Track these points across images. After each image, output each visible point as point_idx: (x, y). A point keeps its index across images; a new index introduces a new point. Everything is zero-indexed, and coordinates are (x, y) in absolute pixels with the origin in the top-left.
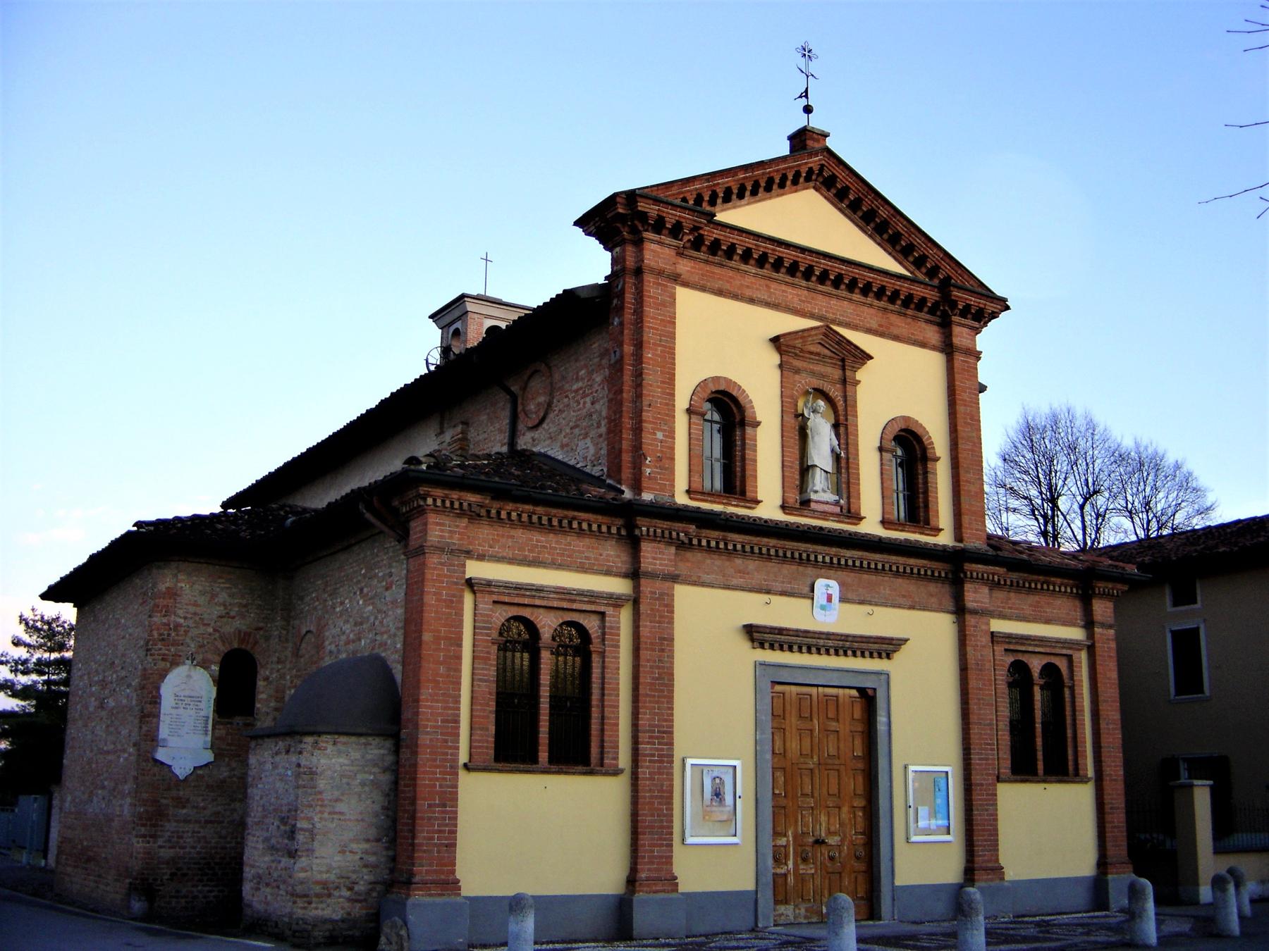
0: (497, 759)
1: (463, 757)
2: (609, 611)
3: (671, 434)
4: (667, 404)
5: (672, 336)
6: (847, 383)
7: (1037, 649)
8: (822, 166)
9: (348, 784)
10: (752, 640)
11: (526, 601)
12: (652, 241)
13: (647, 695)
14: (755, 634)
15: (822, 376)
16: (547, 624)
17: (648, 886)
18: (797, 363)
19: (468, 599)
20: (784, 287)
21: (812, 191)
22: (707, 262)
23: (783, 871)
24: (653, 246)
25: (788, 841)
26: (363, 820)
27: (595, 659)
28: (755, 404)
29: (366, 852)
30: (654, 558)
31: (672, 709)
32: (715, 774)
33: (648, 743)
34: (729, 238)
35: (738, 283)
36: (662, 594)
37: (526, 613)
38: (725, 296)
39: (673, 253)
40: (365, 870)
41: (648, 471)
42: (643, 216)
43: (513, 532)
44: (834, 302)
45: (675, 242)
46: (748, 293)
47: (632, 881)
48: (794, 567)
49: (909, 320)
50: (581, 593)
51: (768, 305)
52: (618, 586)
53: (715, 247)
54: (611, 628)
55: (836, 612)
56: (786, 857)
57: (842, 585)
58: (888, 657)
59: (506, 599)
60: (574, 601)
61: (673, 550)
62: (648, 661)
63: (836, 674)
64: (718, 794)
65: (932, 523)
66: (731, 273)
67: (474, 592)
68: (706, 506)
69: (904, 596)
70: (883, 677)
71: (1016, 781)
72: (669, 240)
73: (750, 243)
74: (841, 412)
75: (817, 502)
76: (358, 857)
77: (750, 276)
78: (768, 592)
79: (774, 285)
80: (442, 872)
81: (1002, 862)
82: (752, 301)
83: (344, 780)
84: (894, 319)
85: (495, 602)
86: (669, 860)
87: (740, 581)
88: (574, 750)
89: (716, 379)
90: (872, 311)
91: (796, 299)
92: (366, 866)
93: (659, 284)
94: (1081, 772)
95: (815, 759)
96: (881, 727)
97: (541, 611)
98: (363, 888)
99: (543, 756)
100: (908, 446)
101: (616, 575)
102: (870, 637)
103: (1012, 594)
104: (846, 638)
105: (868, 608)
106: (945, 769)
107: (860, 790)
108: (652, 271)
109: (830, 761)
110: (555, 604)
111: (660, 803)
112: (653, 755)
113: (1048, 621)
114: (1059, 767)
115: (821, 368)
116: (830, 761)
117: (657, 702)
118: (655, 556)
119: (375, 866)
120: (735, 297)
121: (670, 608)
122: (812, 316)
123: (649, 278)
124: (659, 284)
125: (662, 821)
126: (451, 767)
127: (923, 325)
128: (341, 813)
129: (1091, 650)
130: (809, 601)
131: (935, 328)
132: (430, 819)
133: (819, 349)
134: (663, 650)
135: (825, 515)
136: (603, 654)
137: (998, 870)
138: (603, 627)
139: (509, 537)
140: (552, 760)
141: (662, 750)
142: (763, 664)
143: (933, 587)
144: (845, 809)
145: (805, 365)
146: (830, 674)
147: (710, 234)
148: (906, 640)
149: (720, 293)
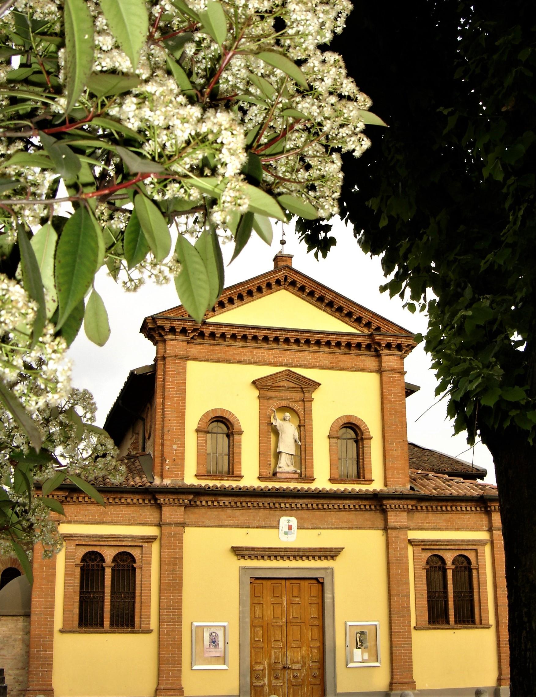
0: (80, 625)
1: (413, 624)
2: (145, 545)
3: (182, 445)
4: (180, 429)
5: (184, 391)
6: (306, 401)
7: (448, 547)
8: (286, 276)
9: (7, 640)
10: (237, 555)
11: (95, 543)
12: (387, 355)
13: (166, 589)
14: (240, 552)
15: (287, 399)
16: (109, 554)
17: (165, 692)
18: (270, 394)
19: (410, 548)
20: (262, 351)
21: (283, 291)
22: (210, 344)
23: (260, 684)
24: (172, 342)
25: (265, 667)
26: (15, 659)
27: (474, 572)
28: (240, 421)
29: (17, 675)
30: (171, 515)
31: (181, 596)
32: (212, 630)
33: (166, 615)
34: (219, 331)
35: (231, 353)
36: (175, 534)
37: (463, 553)
38: (221, 362)
39: (185, 344)
40: (16, 684)
41: (167, 467)
42: (162, 328)
43: (88, 507)
44: (298, 354)
45: (399, 353)
46: (238, 358)
47: (391, 684)
48: (268, 511)
49: (354, 356)
50: (126, 537)
51: (250, 363)
52: (151, 531)
53: (213, 335)
54: (146, 554)
55: (295, 536)
56: (264, 676)
57: (299, 519)
58: (332, 558)
59: (84, 543)
60: (123, 541)
61: (182, 509)
62: (166, 571)
63: (295, 571)
64: (214, 642)
65: (367, 477)
66: (226, 348)
67: (412, 545)
68: (211, 483)
69: (346, 522)
70: (329, 571)
71: (114, 632)
72: (181, 337)
73: (234, 331)
74: (302, 418)
75: (281, 473)
76: (13, 677)
77: (239, 349)
78: (248, 527)
79: (255, 351)
80: (44, 685)
81: (415, 678)
82: (239, 362)
83: (5, 639)
84: (341, 357)
85: (77, 545)
86: (179, 678)
87: (230, 522)
88: (125, 619)
89: (223, 410)
90: (326, 355)
91: (271, 357)
92: (17, 682)
93: (176, 363)
94: (483, 622)
95: (284, 620)
96: (327, 600)
97: (105, 547)
98: (15, 693)
99: (107, 623)
100: (352, 430)
101: (151, 525)
102: (316, 549)
103: (430, 515)
104: (299, 550)
105: (317, 531)
106: (225, 624)
107: (316, 637)
108: (171, 357)
109: (294, 621)
110: (112, 544)
111: (172, 648)
112: (169, 622)
113: (458, 529)
114: (467, 616)
115: (288, 395)
116: (274, 621)
117: (172, 593)
118: (172, 513)
119: (22, 682)
120: (229, 362)
121: (181, 541)
122: (281, 365)
123: (169, 361)
124: (176, 363)
125: (174, 657)
126: (49, 631)
127: (364, 358)
128: (3, 655)
129: (492, 543)
130: (278, 530)
131: (373, 358)
132: (37, 658)
133: (286, 384)
134: (176, 564)
135: (288, 480)
136: (477, 569)
137: (412, 684)
138: (142, 554)
139: (88, 510)
140: (112, 625)
141: (175, 618)
142: (244, 568)
143: (367, 515)
144: (305, 648)
145: (276, 393)
146: (291, 571)
147: (207, 330)
148: (343, 549)
149: (218, 361)
